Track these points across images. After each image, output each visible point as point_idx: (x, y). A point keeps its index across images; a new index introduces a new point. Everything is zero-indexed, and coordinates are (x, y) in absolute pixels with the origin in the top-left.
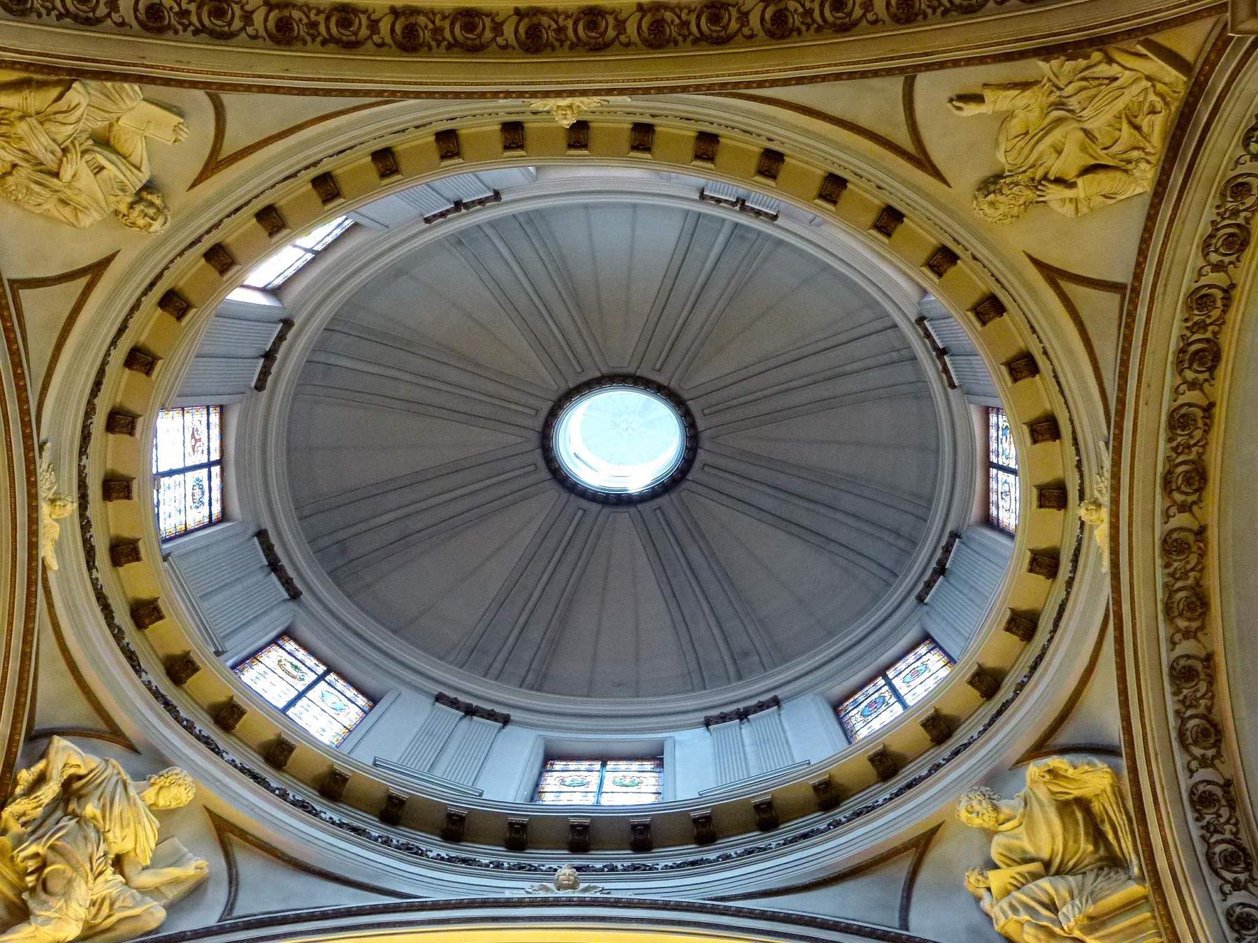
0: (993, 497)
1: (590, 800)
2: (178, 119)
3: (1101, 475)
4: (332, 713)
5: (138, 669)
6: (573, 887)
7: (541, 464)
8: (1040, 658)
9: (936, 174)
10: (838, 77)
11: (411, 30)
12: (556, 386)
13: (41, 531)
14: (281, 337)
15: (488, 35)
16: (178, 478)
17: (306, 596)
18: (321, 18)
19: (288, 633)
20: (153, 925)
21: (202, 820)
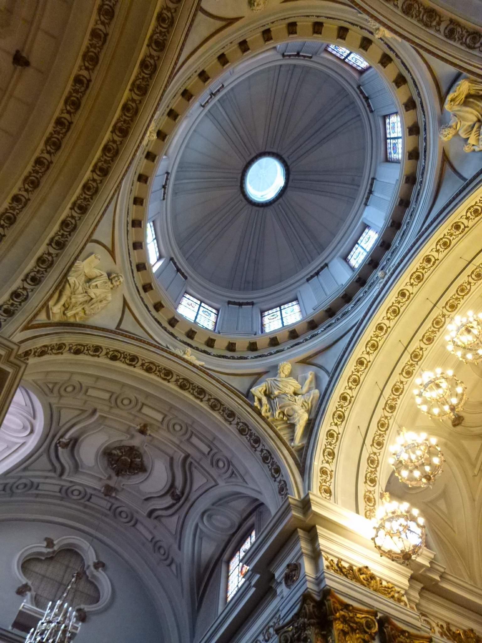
0: (355, 66)
1: (365, 254)
2: (93, 256)
3: (369, 22)
4: (293, 313)
5: (245, 358)
6: (386, 274)
7: (257, 208)
8: (414, 82)
9: (237, 19)
10: (187, 35)
11: (101, 170)
12: (237, 190)
13: (191, 361)
14: (175, 264)
15: (115, 146)
16: (199, 316)
17: (255, 301)
18: (84, 195)
19: (262, 312)
20: (318, 395)
21: (299, 367)
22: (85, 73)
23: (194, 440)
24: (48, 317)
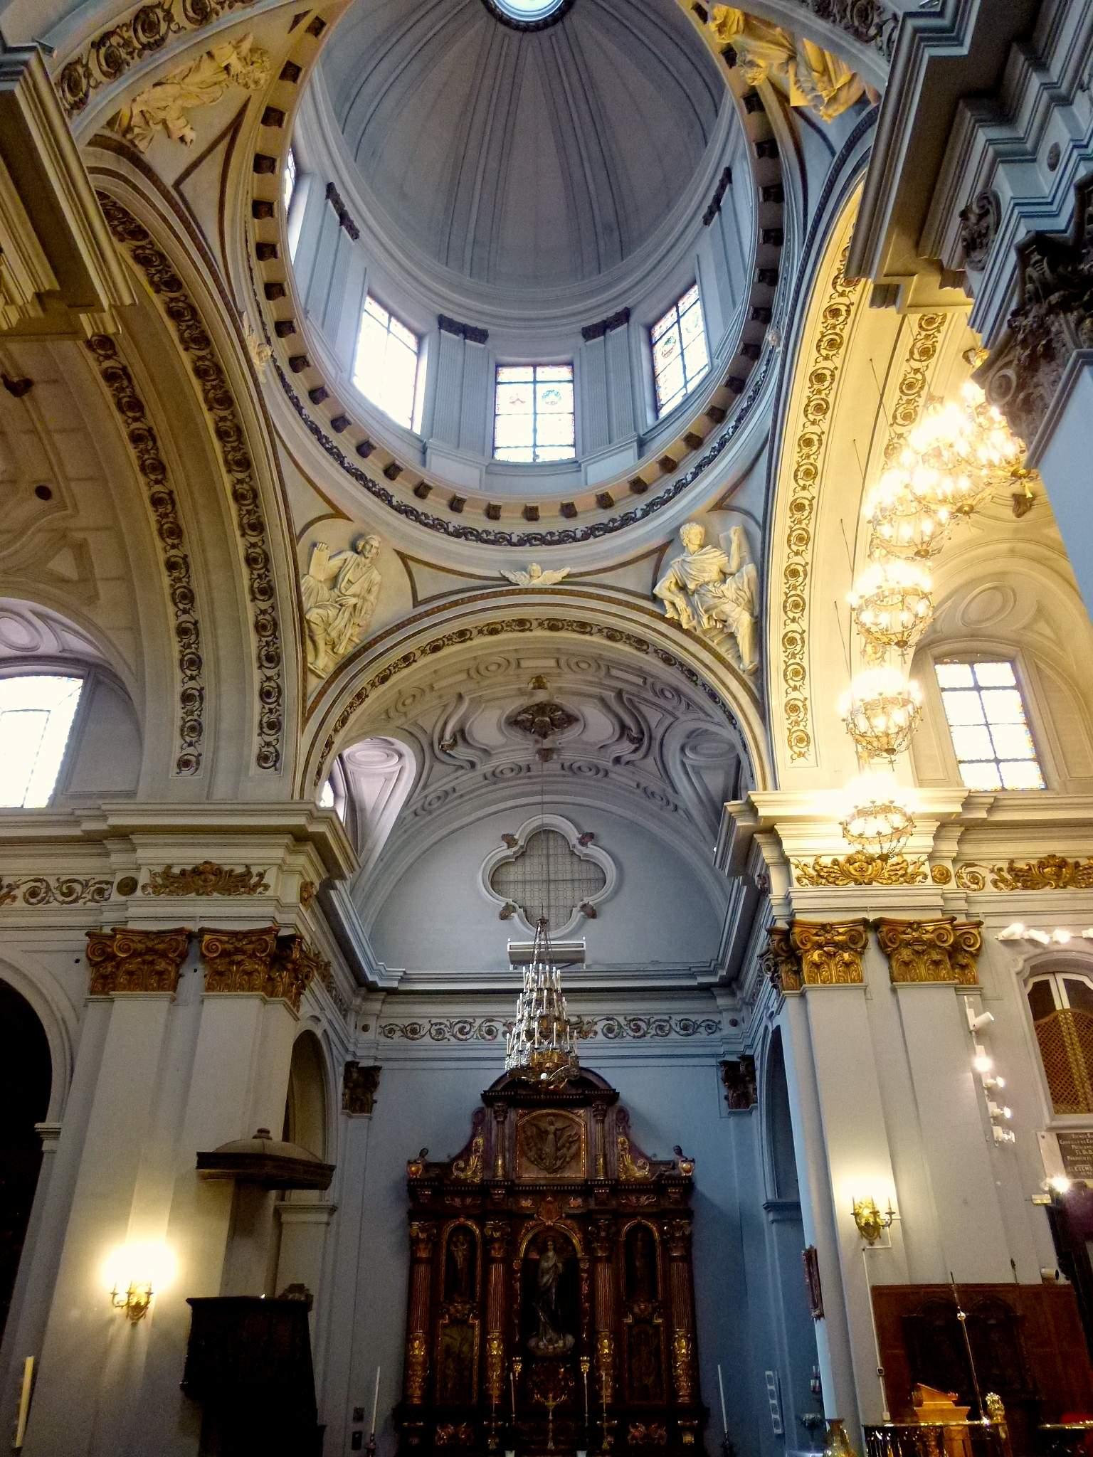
7: (550, 30)
23: (614, 672)
24: (319, 677)
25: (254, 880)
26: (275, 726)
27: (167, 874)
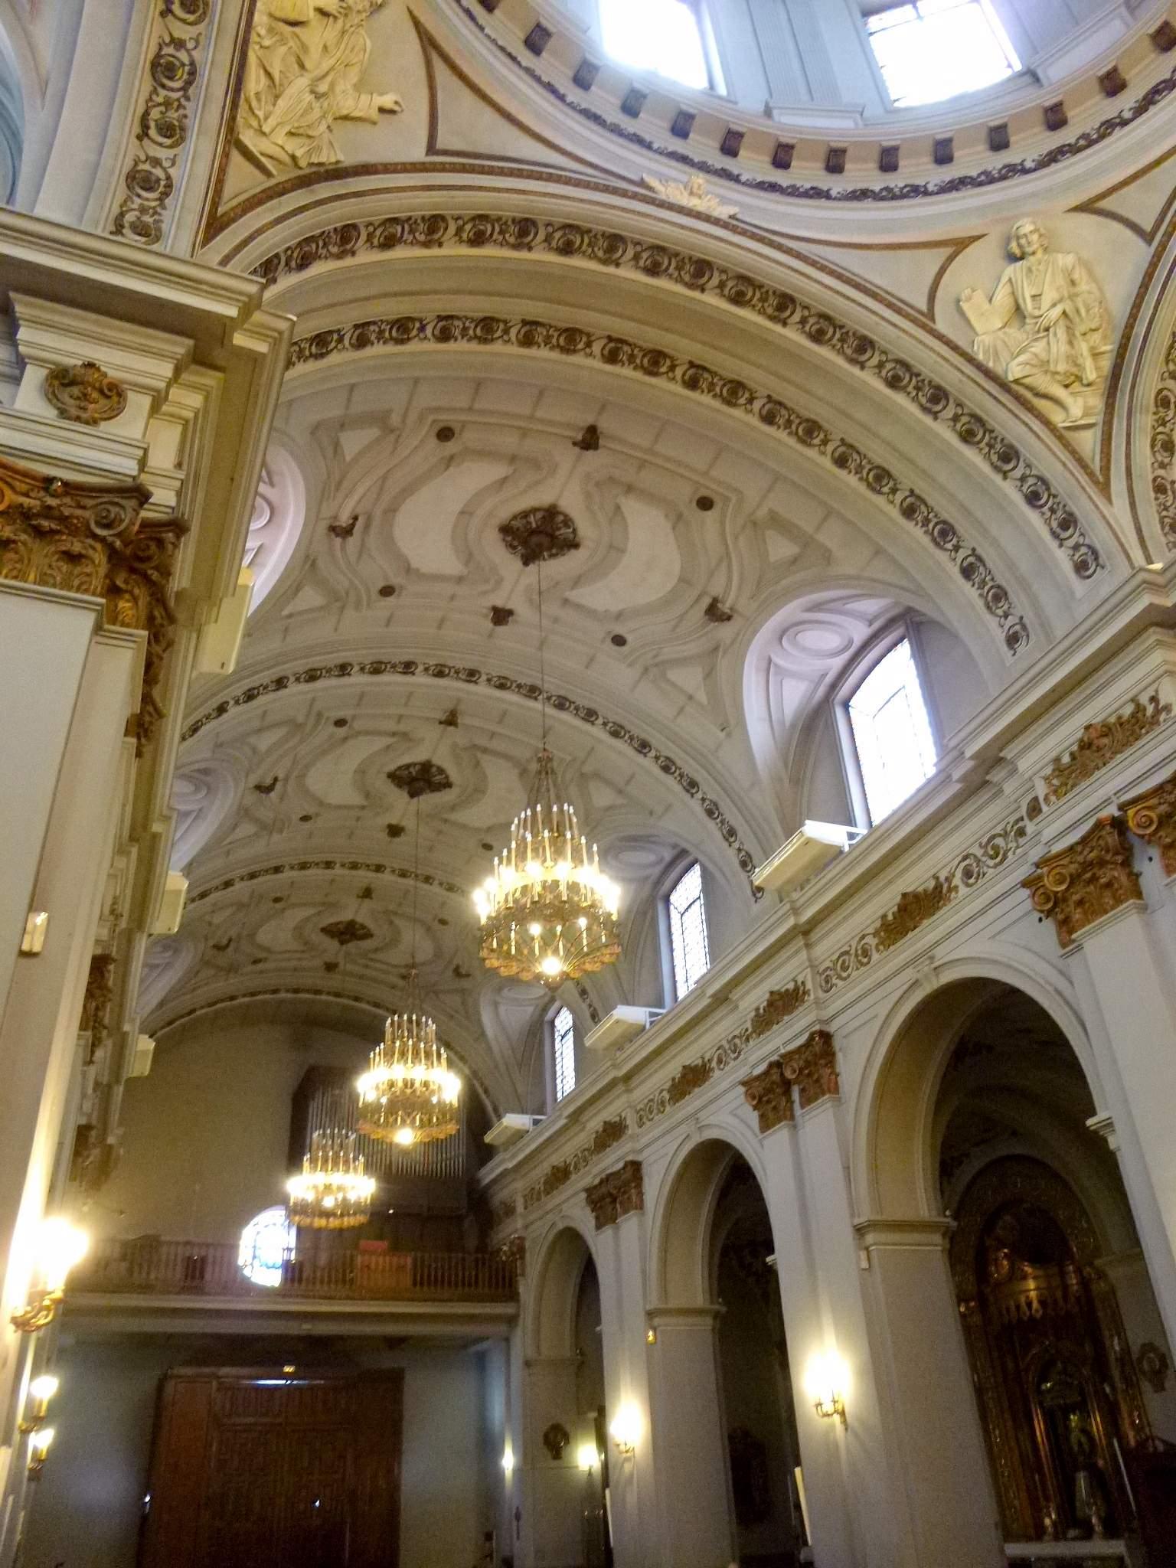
2: (965, 306)
22: (597, 348)
25: (1150, 709)
26: (1069, 522)
27: (1059, 770)
